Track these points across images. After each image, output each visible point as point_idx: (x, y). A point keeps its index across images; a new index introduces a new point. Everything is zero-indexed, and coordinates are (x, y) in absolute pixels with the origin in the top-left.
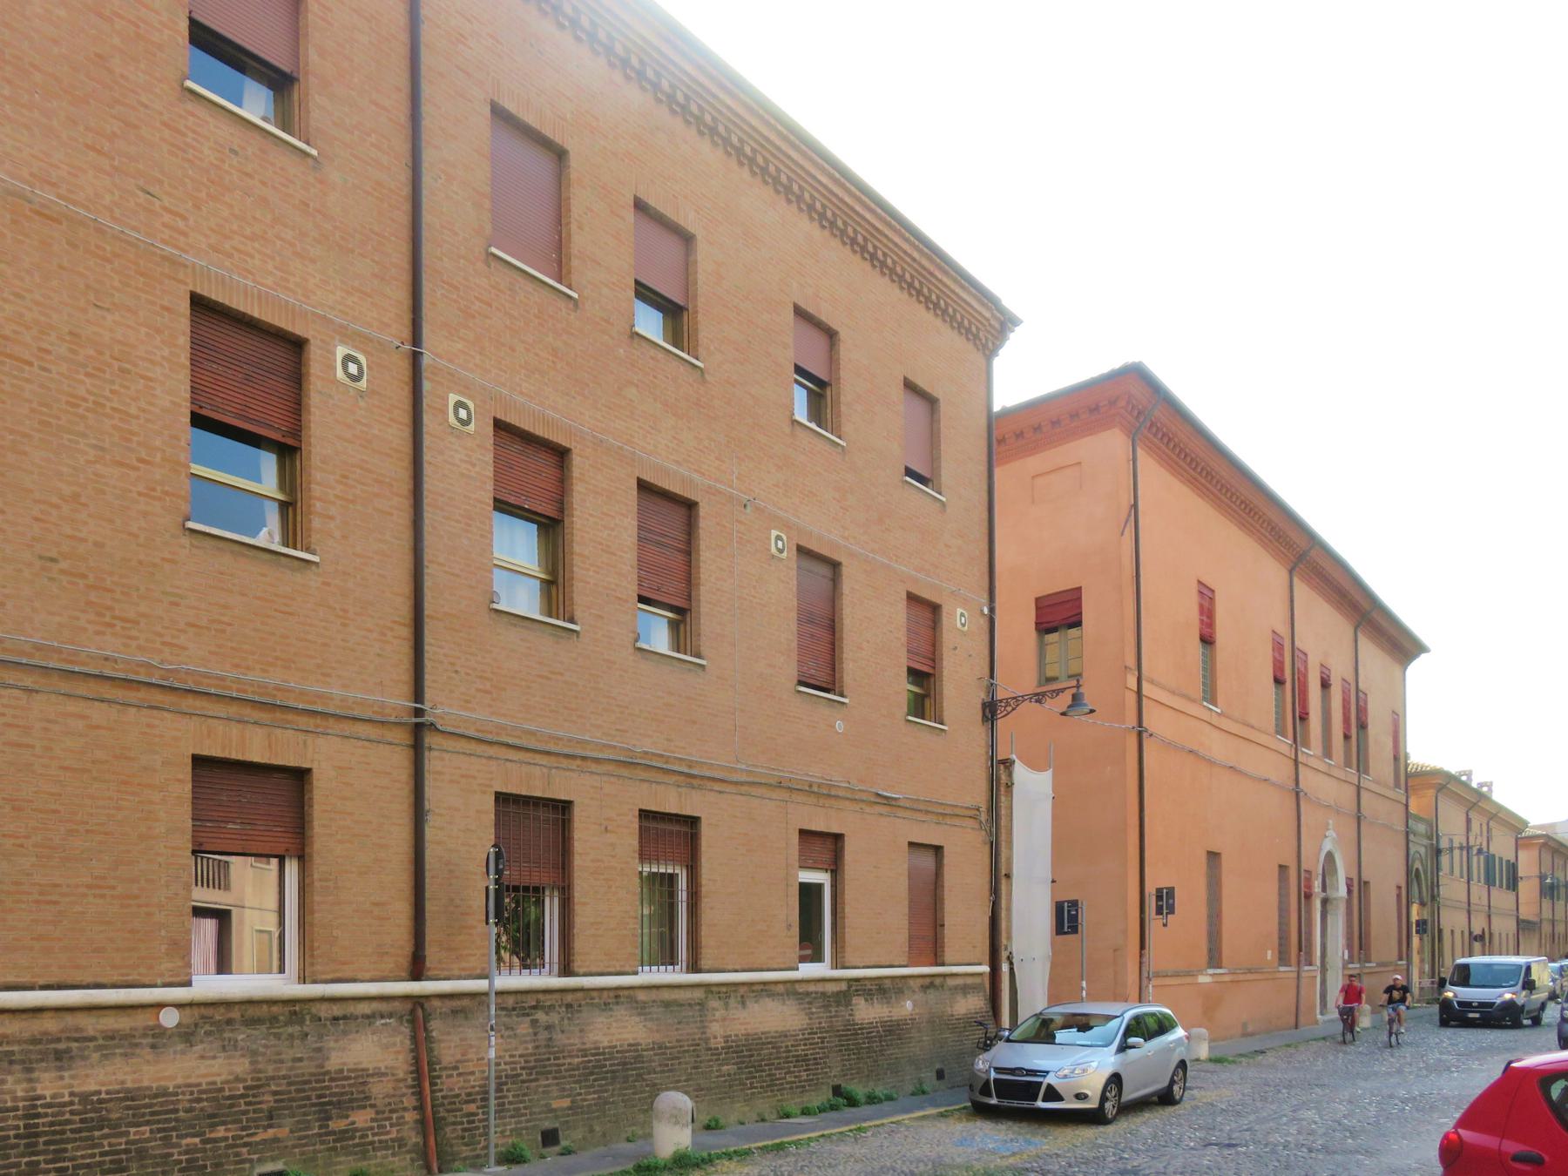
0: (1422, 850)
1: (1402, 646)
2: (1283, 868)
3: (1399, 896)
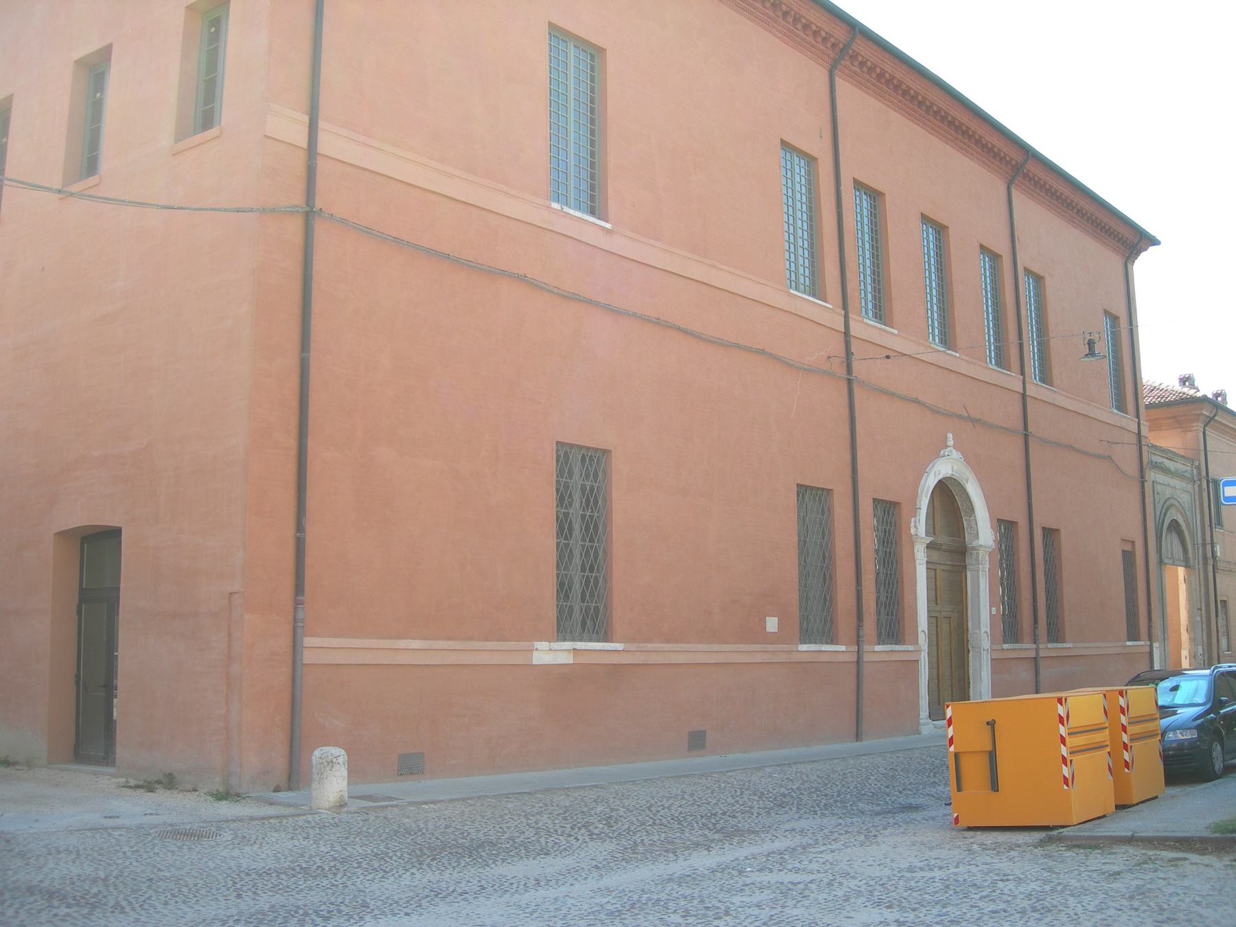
0: (1185, 499)
1: (1130, 240)
2: (812, 499)
3: (1128, 557)
